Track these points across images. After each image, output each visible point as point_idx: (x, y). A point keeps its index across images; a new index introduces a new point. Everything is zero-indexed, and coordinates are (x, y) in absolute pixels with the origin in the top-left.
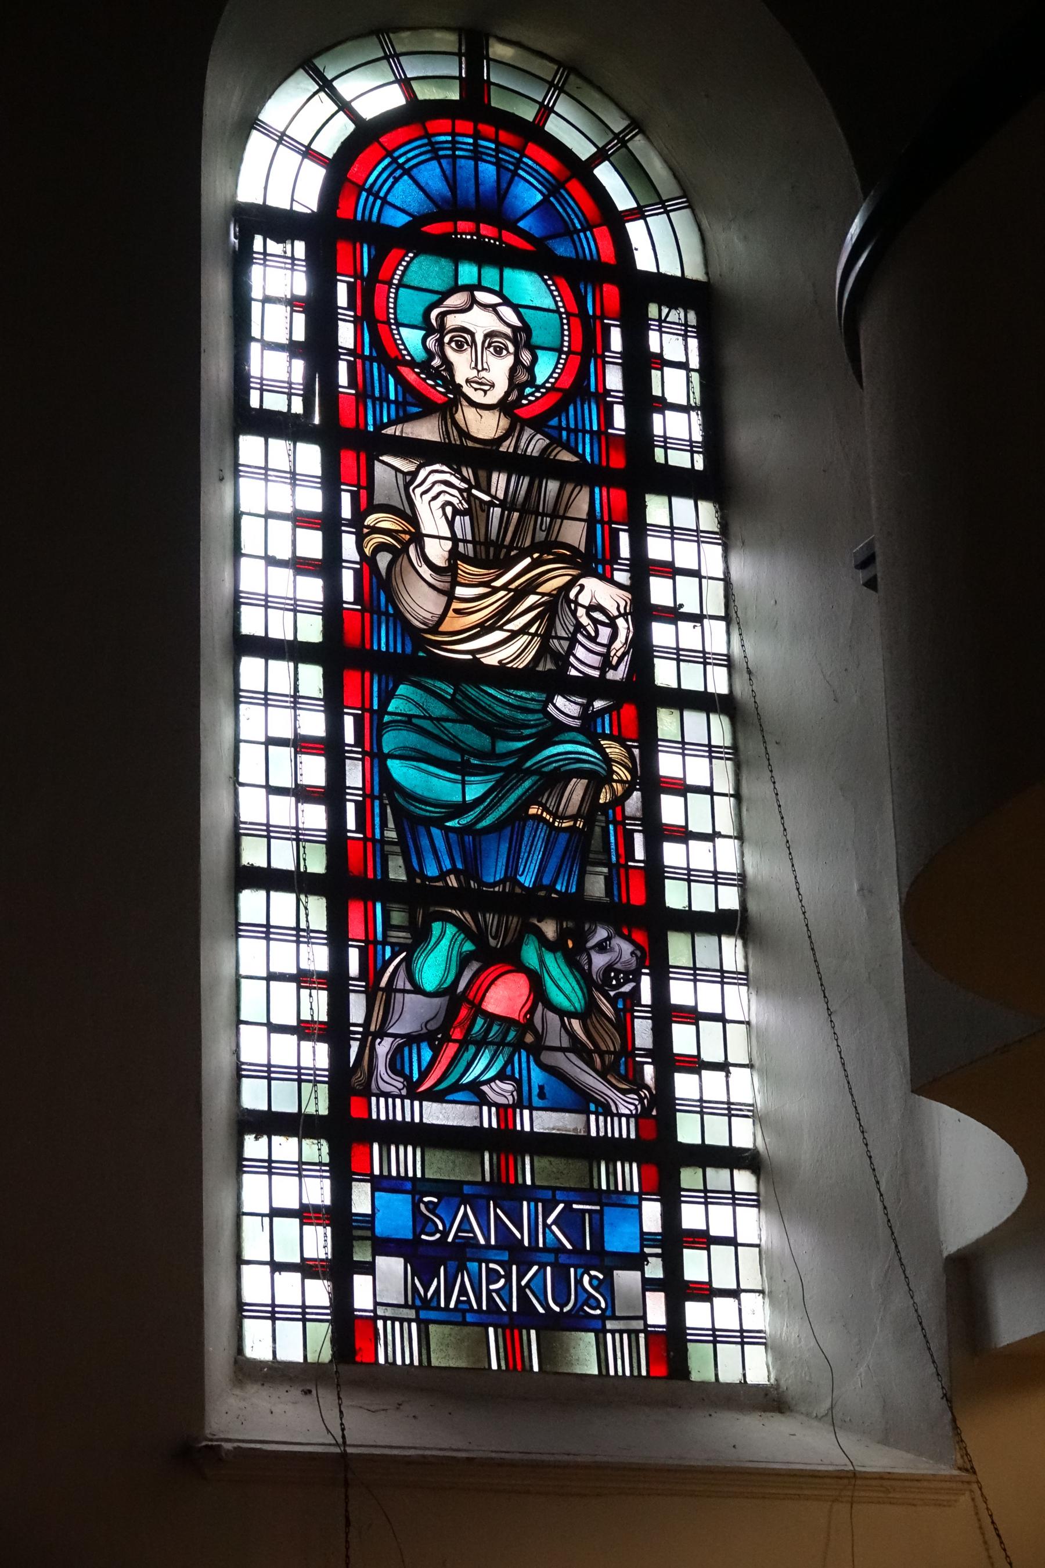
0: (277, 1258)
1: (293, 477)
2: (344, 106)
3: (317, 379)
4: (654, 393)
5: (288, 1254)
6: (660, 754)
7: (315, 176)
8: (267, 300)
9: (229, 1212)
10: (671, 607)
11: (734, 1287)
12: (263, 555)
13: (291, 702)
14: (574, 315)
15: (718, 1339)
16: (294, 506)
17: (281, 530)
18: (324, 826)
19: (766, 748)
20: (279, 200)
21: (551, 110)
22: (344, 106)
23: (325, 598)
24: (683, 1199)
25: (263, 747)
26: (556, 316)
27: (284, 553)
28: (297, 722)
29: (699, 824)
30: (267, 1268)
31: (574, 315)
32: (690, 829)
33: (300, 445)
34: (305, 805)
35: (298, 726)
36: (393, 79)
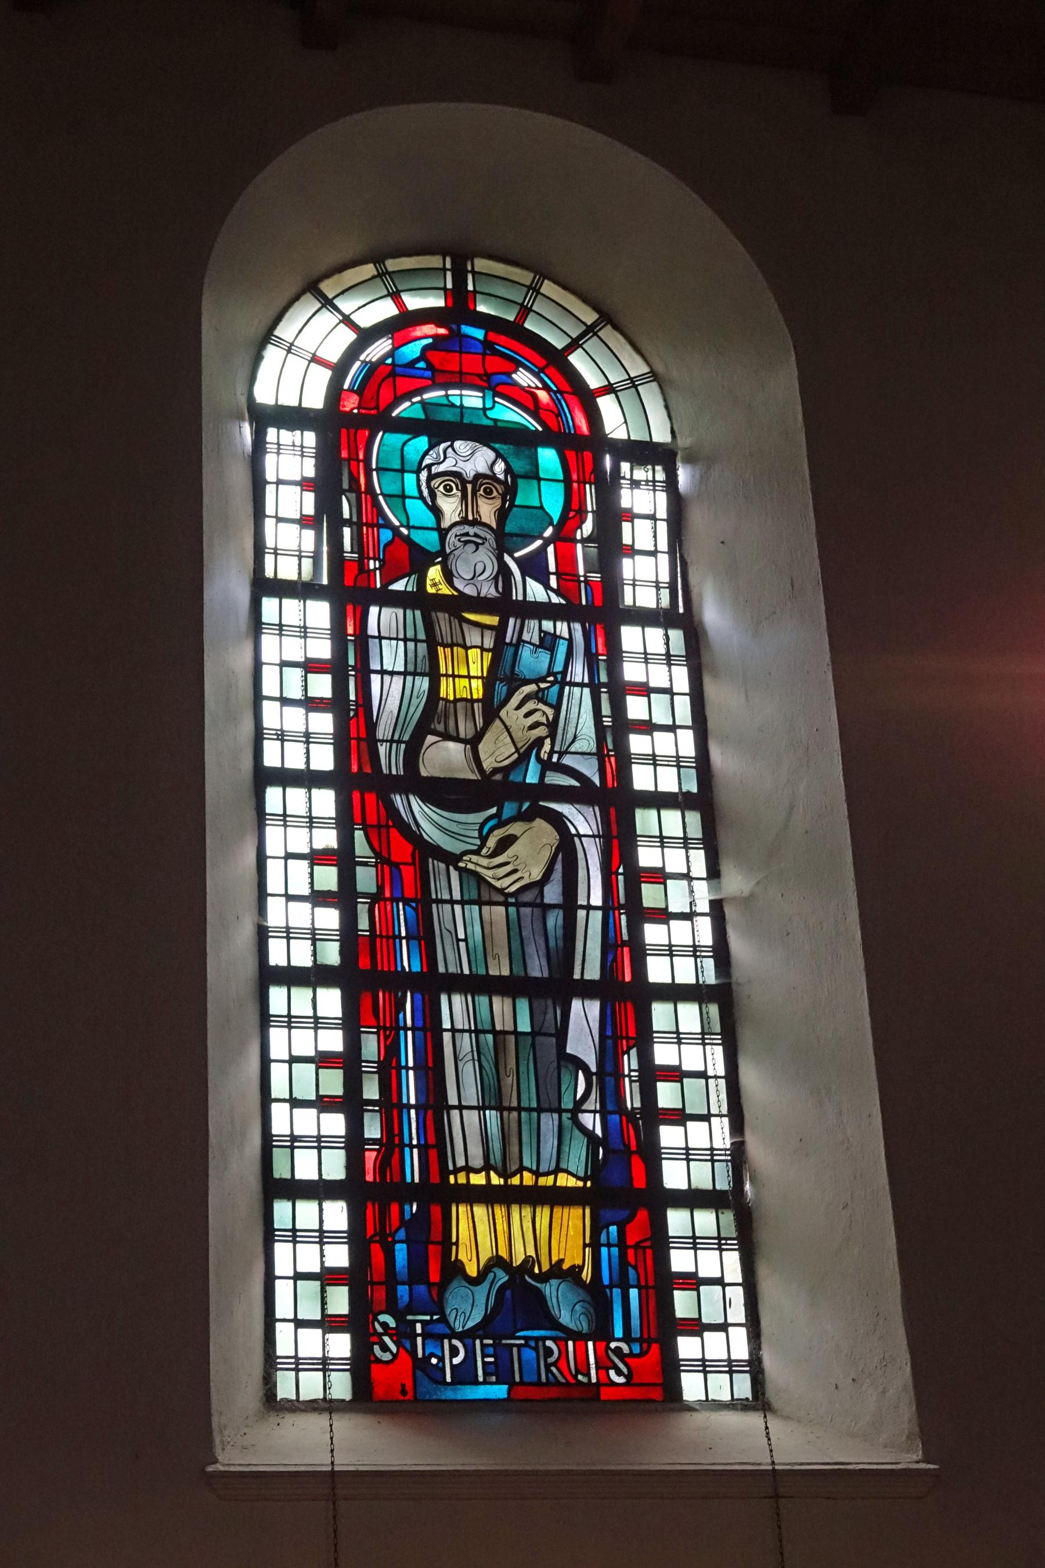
0: (290, 892)
1: (304, 632)
2: (347, 320)
3: (325, 524)
4: (625, 542)
5: (294, 692)
6: (639, 848)
7: (322, 377)
8: (279, 482)
9: (246, 931)
10: (625, 440)
11: (706, 1112)
12: (287, 1097)
13: (307, 822)
14: (546, 367)
15: (701, 1363)
16: (302, 475)
17: (305, 1072)
18: (343, 1132)
19: (766, 1423)
20: (289, 399)
21: (530, 310)
22: (347, 320)
23: (334, 731)
24: (648, 952)
25: (287, 1065)
26: (544, 672)
27: (313, 1266)
28: (308, 806)
29: (661, 717)
30: (284, 899)
31: (546, 367)
32: (654, 721)
33: (310, 603)
34: (330, 1335)
35: (308, 804)
36: (386, 293)
